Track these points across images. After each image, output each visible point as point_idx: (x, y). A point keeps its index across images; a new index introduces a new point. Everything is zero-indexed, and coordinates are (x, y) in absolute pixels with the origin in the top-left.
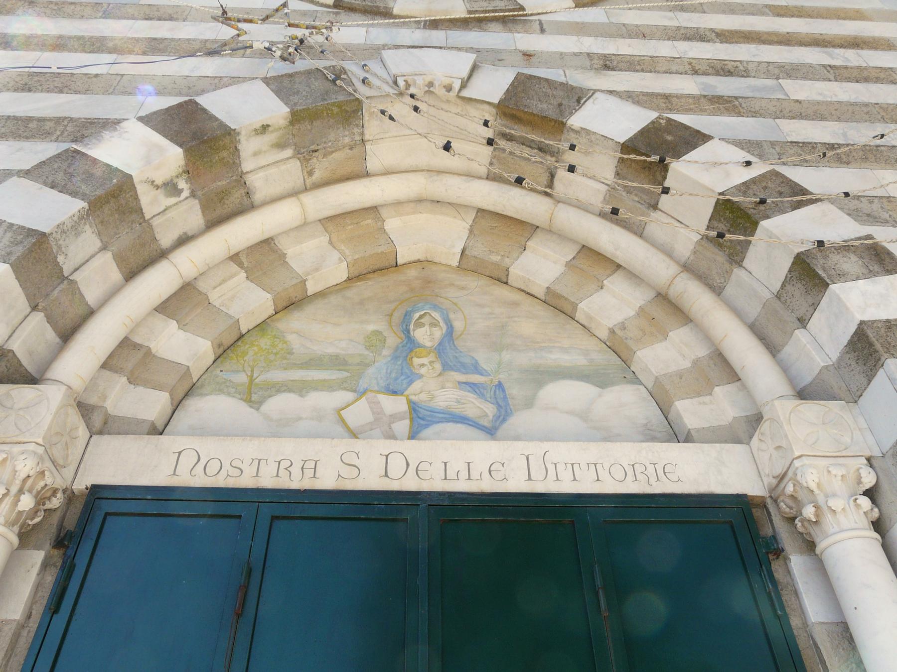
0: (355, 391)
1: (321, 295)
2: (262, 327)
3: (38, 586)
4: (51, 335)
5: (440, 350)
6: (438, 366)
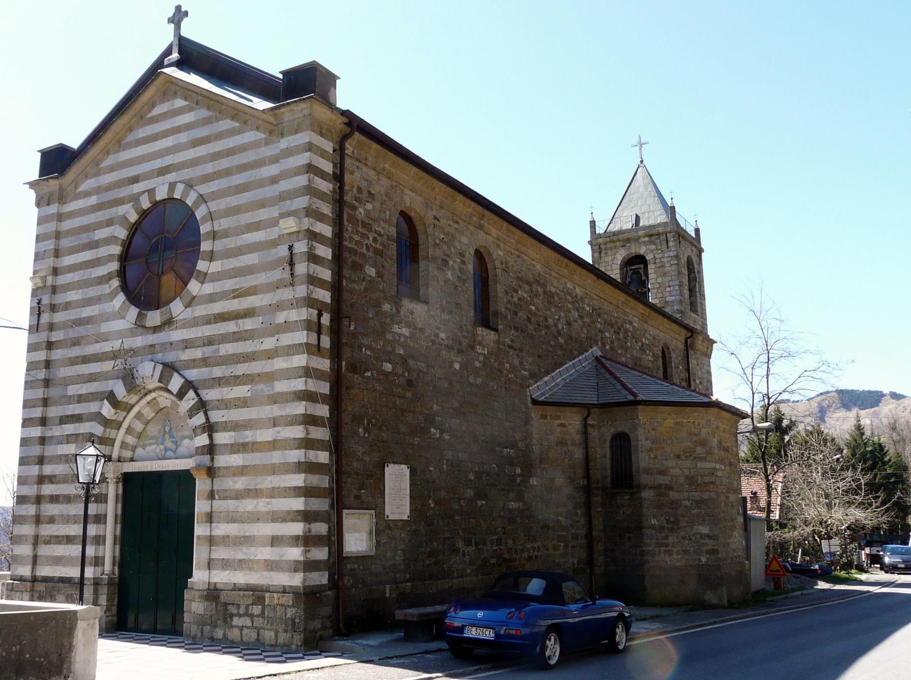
1: (152, 419)
2: (144, 429)
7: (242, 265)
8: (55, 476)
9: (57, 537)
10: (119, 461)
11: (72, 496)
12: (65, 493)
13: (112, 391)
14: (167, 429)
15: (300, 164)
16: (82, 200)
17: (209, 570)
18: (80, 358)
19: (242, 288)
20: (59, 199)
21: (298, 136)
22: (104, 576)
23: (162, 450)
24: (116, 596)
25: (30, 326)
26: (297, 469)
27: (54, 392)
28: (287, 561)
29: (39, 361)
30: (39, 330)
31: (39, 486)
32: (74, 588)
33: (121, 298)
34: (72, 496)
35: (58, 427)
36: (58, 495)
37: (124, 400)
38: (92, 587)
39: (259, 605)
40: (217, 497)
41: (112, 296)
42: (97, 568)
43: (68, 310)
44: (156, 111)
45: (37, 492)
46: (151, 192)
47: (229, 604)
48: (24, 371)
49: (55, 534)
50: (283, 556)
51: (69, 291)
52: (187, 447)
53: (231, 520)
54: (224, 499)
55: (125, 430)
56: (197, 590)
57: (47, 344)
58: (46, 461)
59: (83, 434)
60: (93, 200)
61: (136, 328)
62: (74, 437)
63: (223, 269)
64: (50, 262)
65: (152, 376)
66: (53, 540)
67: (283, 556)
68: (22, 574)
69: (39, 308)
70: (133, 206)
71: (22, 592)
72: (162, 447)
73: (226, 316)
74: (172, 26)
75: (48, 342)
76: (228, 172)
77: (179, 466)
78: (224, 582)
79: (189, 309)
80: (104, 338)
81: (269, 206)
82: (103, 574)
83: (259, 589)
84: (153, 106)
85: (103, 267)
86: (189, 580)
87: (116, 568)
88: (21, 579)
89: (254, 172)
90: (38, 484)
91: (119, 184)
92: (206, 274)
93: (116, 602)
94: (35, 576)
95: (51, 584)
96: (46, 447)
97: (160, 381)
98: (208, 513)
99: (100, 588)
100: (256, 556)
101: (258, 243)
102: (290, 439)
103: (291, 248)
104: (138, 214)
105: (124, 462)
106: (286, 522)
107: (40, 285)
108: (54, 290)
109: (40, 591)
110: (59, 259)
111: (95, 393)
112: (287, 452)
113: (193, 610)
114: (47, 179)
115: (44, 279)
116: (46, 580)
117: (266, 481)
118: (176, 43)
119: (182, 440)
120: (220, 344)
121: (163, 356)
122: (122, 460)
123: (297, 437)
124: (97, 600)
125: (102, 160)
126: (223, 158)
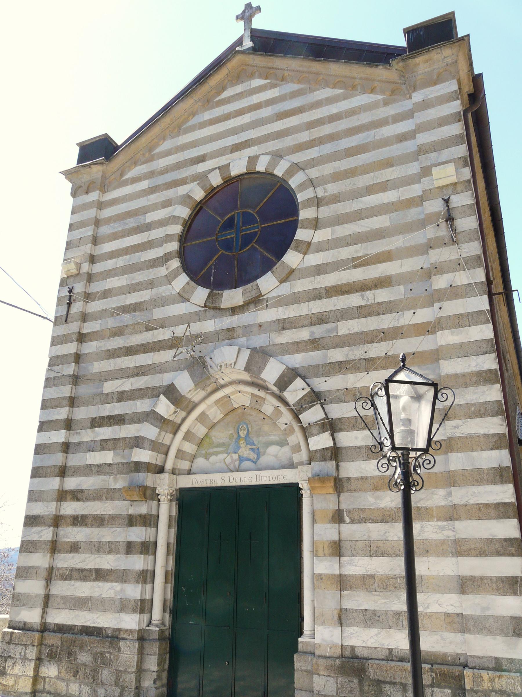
0: (227, 453)
1: (219, 422)
2: (207, 435)
3: (176, 508)
4: (163, 456)
5: (245, 438)
6: (245, 444)
7: (364, 229)
8: (82, 491)
9: (81, 570)
10: (173, 473)
11: (107, 517)
12: (96, 513)
13: (172, 384)
14: (243, 434)
15: (447, 114)
16: (129, 186)
17: (341, 626)
18: (123, 350)
19: (368, 255)
20: (101, 186)
21: (438, 87)
22: (152, 628)
23: (236, 460)
24: (168, 656)
25: (56, 318)
26: (498, 478)
27: (84, 390)
28: (497, 618)
29: (67, 355)
30: (68, 321)
31: (59, 503)
32: (107, 644)
33: (183, 279)
34: (107, 517)
35: (89, 431)
36: (86, 515)
37: (189, 396)
38: (136, 645)
39: (445, 687)
40: (347, 519)
41: (170, 278)
42: (142, 615)
43: (107, 298)
44: (225, 94)
45: (56, 512)
46: (224, 169)
47: (386, 683)
48: (47, 367)
49: (78, 566)
50: (488, 608)
51: (110, 278)
52: (276, 456)
53: (376, 552)
54: (360, 522)
55: (184, 434)
56: (320, 657)
57: (79, 336)
58: (67, 472)
59: (125, 439)
60: (145, 184)
61: (206, 311)
62: (112, 442)
63: (335, 237)
64: (88, 248)
65: (235, 363)
66: (75, 574)
67: (488, 608)
68: (27, 620)
69: (70, 296)
70: (198, 184)
71: (26, 646)
72: (235, 457)
73: (344, 289)
74: (242, 23)
75: (79, 332)
76: (332, 138)
77: (263, 480)
78: (369, 645)
79: (286, 285)
80: (163, 324)
81: (398, 165)
82: (150, 623)
83: (439, 661)
84: (224, 89)
85: (156, 250)
86: (300, 639)
87: (167, 616)
88: (25, 627)
89: (372, 132)
90: (57, 501)
91: (179, 166)
92: (309, 244)
93: (166, 666)
94: (45, 623)
95: (69, 636)
96: (70, 456)
97: (247, 369)
98: (334, 543)
99: (146, 645)
100: (428, 607)
101: (387, 204)
102: (479, 436)
103: (447, 201)
104: (223, 180)
105: (179, 475)
106: (486, 555)
107: (74, 271)
108: (90, 278)
109: (52, 645)
110: (98, 247)
111: (144, 389)
112: (475, 454)
113: (316, 688)
114: (90, 165)
115: (79, 266)
116: (61, 629)
117: (435, 496)
118: (248, 33)
119: (267, 447)
120: (338, 321)
121: (248, 340)
122: (177, 472)
123: (492, 432)
124: (141, 663)
125: (157, 145)
126: (324, 124)
